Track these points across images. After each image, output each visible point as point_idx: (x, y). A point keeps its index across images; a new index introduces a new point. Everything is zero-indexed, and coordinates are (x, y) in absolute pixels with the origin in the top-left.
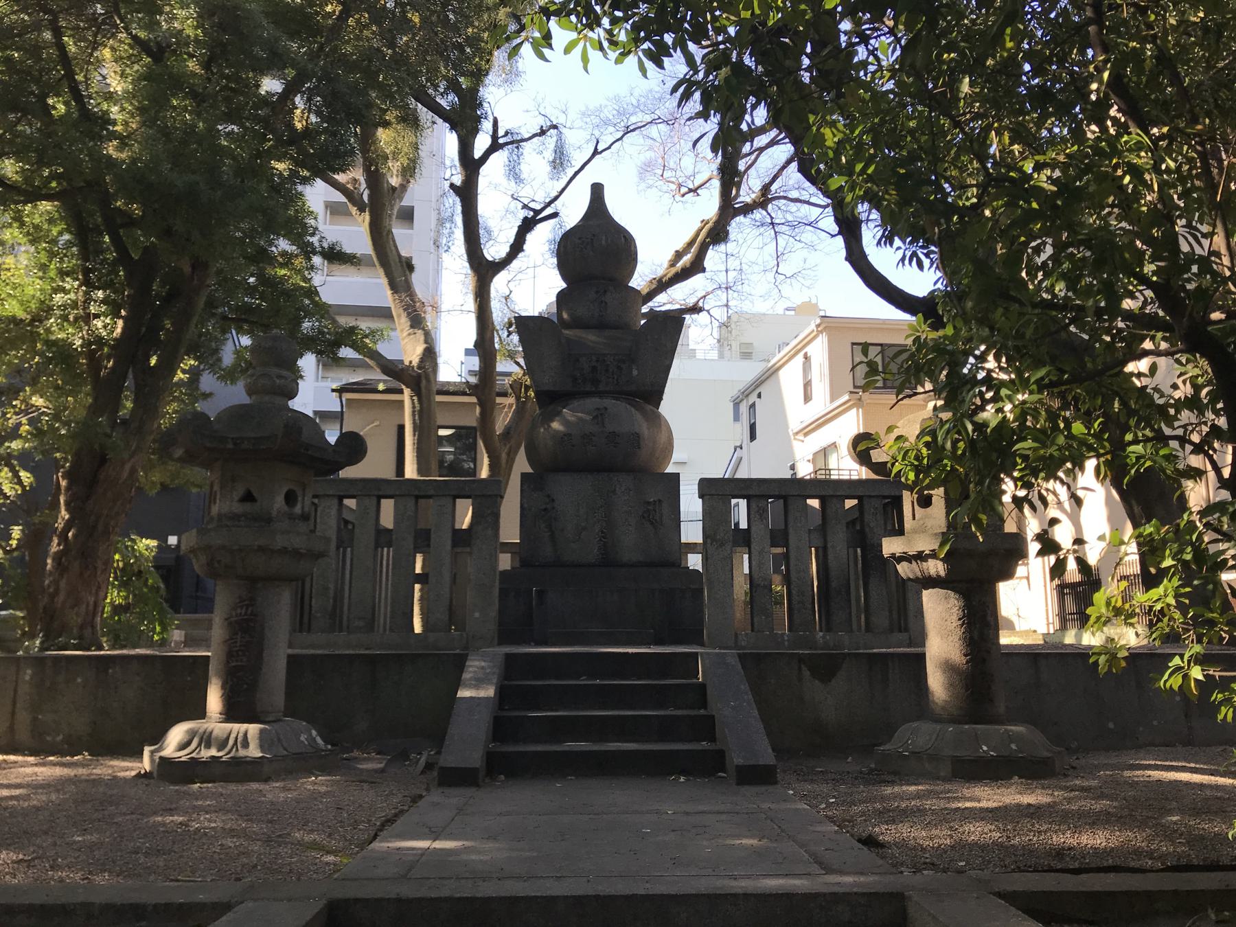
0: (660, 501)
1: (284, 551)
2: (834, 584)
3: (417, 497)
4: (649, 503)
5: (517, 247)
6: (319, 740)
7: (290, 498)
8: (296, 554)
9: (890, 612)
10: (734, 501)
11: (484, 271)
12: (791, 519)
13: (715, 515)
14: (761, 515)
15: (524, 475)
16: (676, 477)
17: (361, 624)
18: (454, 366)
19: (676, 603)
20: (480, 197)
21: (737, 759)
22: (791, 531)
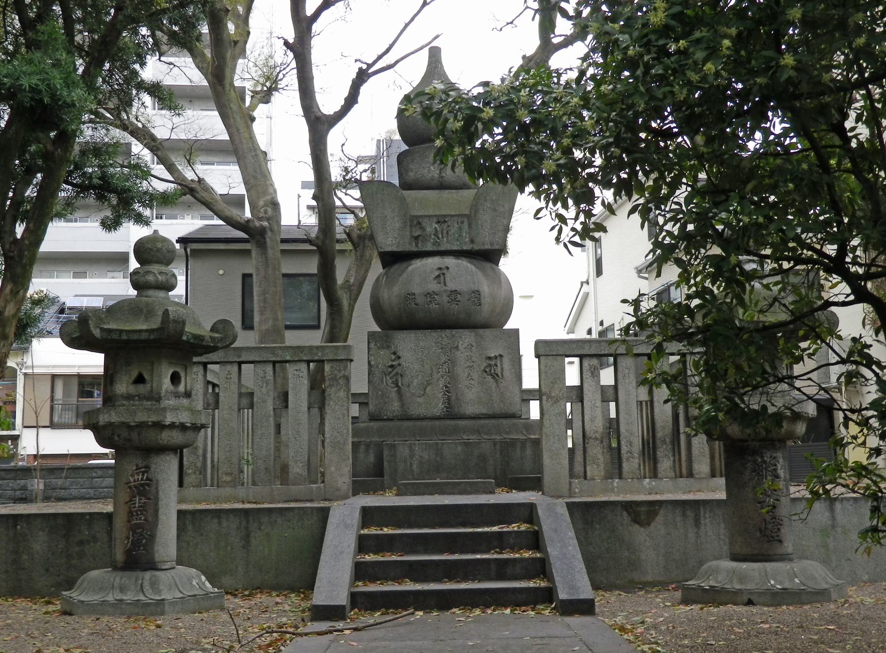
0: (501, 356)
1: (172, 426)
2: (659, 435)
3: (274, 363)
4: (490, 358)
5: (351, 100)
6: (208, 584)
7: (175, 379)
8: (183, 427)
9: (712, 457)
10: (567, 360)
11: (319, 126)
12: (620, 376)
13: (551, 372)
14: (592, 373)
15: (371, 335)
16: (516, 332)
17: (228, 479)
18: (296, 210)
19: (514, 457)
20: (313, 51)
21: (563, 595)
22: (620, 386)
